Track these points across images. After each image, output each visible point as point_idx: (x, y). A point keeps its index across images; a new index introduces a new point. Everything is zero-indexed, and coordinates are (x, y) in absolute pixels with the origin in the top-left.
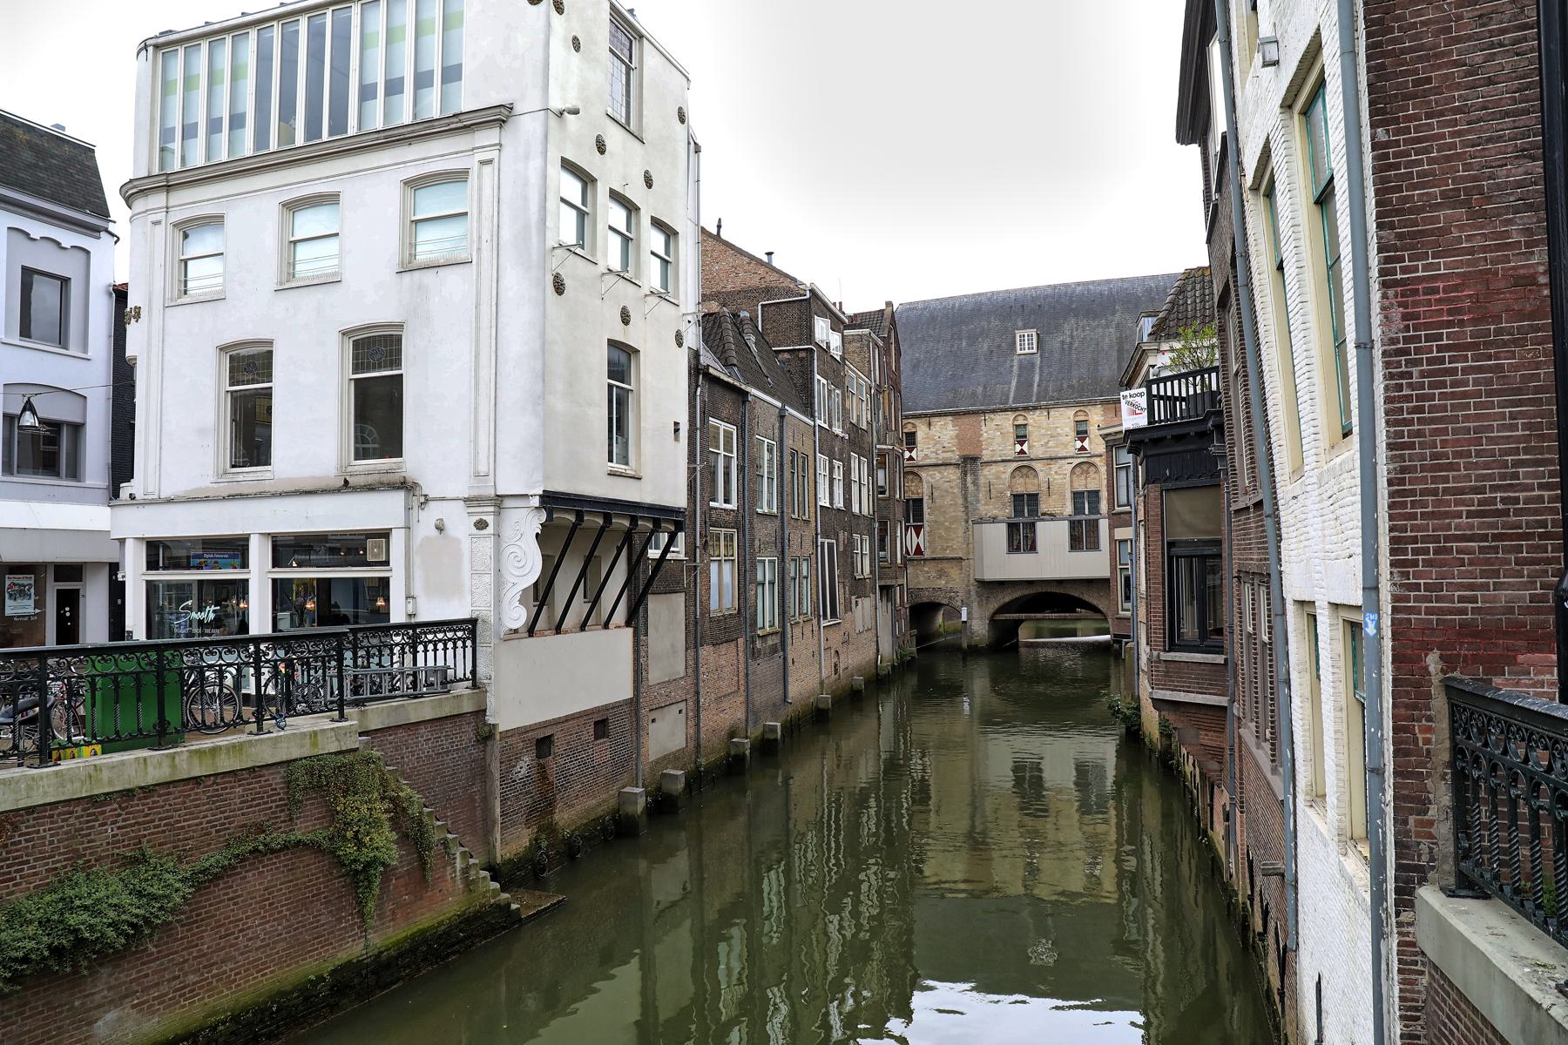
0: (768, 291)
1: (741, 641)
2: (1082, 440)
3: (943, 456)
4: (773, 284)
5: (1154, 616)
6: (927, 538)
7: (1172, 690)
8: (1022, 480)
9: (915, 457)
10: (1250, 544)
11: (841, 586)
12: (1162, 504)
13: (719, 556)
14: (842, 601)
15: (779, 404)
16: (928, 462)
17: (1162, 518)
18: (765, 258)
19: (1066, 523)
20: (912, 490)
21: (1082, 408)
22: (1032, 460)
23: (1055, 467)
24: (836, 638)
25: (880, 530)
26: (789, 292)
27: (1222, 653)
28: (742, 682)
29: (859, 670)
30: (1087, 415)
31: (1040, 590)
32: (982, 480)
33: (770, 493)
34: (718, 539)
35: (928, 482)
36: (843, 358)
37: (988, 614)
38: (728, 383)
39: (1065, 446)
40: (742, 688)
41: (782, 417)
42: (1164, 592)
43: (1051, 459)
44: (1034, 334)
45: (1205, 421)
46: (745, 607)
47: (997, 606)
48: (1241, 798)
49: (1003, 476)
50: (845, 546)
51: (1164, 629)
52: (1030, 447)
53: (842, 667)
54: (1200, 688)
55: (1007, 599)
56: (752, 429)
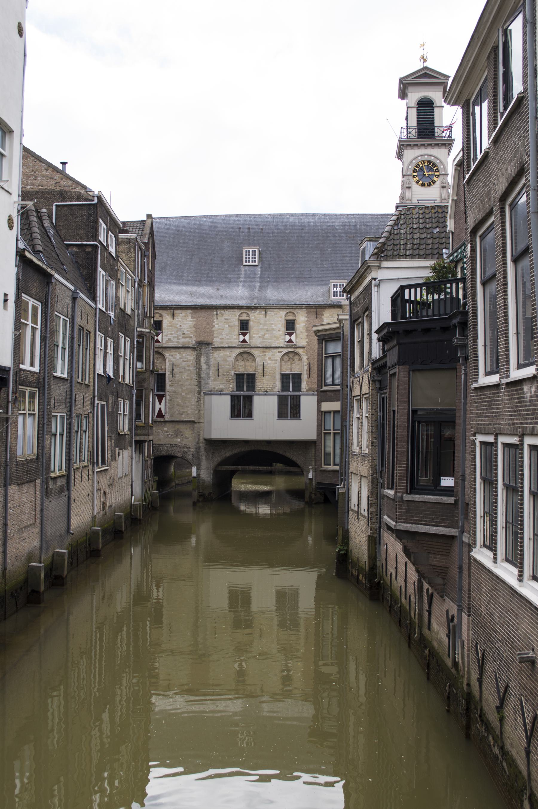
0: (62, 195)
1: (38, 481)
2: (290, 334)
3: (182, 341)
4: (66, 189)
5: (399, 467)
6: (167, 405)
7: (412, 523)
8: (243, 363)
9: (160, 340)
10: (477, 413)
11: (109, 439)
12: (409, 381)
13: (24, 410)
14: (109, 452)
15: (72, 288)
16: (170, 344)
17: (409, 392)
18: (60, 167)
19: (276, 398)
20: (159, 366)
21: (292, 310)
22: (252, 348)
23: (269, 354)
24: (105, 481)
25: (137, 397)
26: (79, 197)
27: (452, 496)
28: (38, 516)
29: (120, 508)
30: (295, 316)
31: (253, 448)
32: (212, 362)
33: (63, 361)
34: (24, 397)
35: (170, 361)
36: (117, 256)
37: (213, 465)
38: (38, 265)
39: (277, 338)
40: (38, 521)
41: (74, 299)
42: (408, 448)
43: (266, 348)
44: (257, 250)
45: (451, 318)
46: (43, 454)
47: (219, 459)
48: (469, 605)
49: (229, 359)
50: (113, 407)
51: (407, 477)
52: (250, 338)
53: (108, 505)
54: (433, 522)
55: (228, 454)
56: (52, 306)
